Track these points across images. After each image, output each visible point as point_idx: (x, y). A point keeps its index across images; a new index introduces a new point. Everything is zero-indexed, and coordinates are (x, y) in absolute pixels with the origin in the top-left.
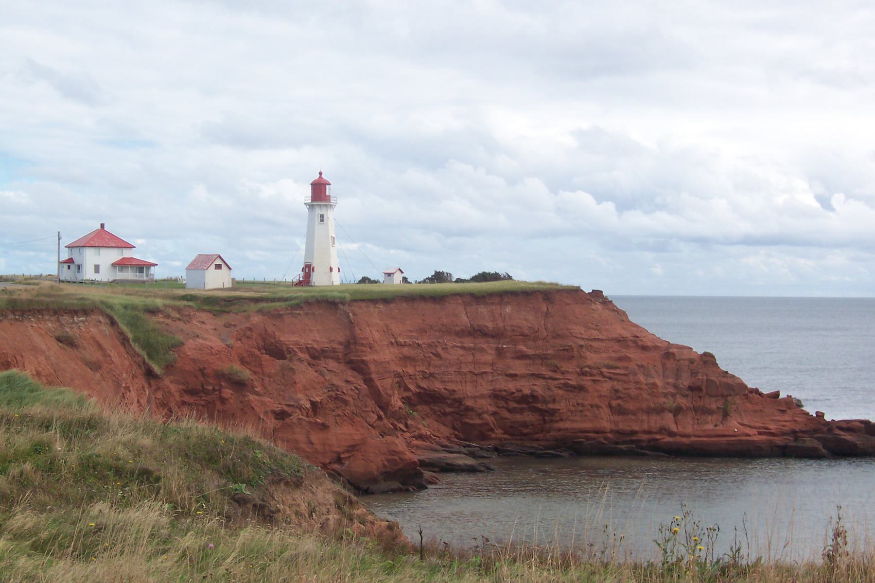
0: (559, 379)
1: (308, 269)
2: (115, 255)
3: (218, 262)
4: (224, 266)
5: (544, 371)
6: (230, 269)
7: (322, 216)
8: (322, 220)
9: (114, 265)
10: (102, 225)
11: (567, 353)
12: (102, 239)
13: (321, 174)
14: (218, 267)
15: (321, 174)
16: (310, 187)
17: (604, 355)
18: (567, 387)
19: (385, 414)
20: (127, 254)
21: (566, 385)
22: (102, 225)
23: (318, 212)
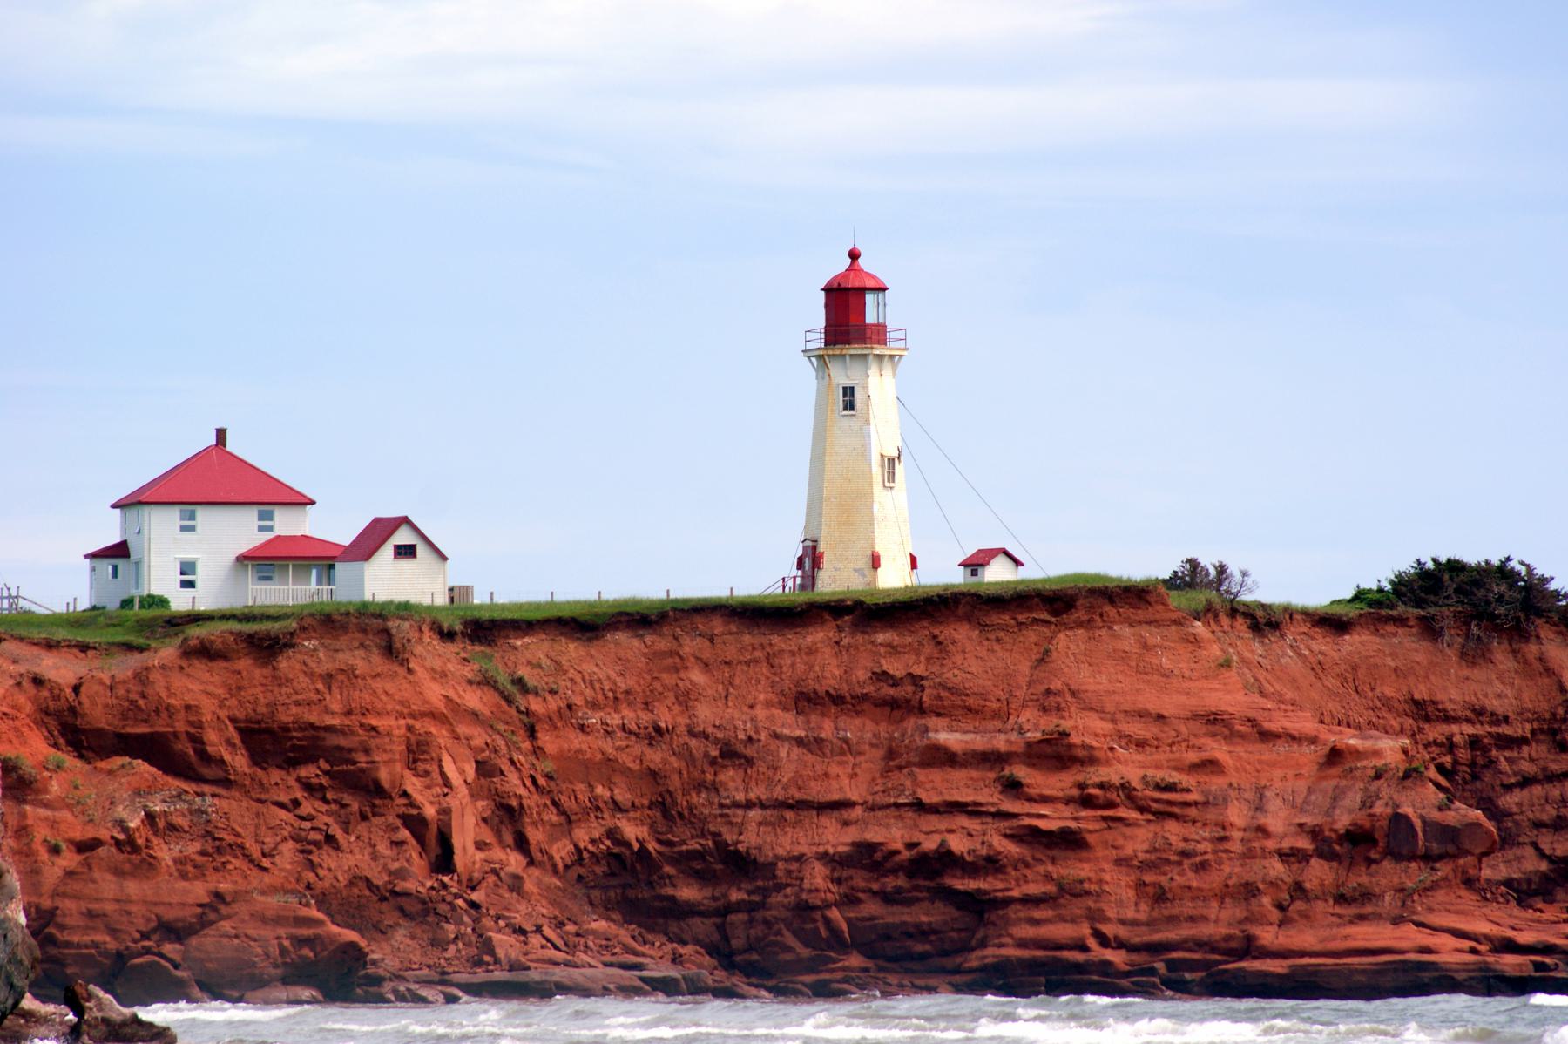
0: (1015, 816)
1: (811, 559)
2: (236, 531)
3: (403, 537)
4: (421, 550)
5: (989, 796)
6: (444, 558)
7: (849, 392)
8: (850, 406)
9: (243, 559)
10: (221, 434)
11: (1055, 753)
12: (212, 479)
13: (854, 255)
14: (406, 552)
15: (854, 255)
16: (821, 297)
17: (1161, 757)
18: (1033, 836)
19: (328, 914)
20: (287, 523)
21: (1035, 832)
22: (221, 434)
23: (841, 376)
